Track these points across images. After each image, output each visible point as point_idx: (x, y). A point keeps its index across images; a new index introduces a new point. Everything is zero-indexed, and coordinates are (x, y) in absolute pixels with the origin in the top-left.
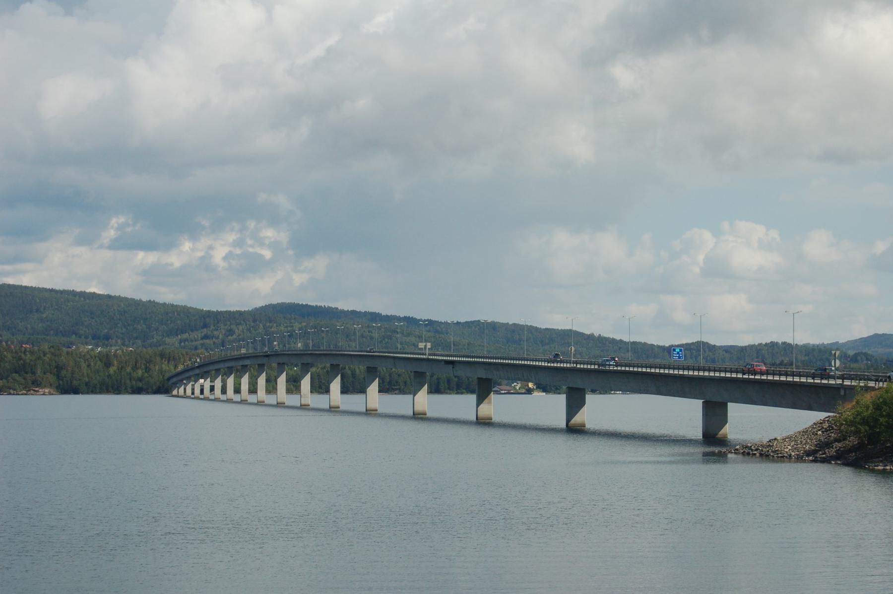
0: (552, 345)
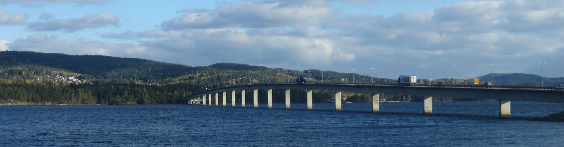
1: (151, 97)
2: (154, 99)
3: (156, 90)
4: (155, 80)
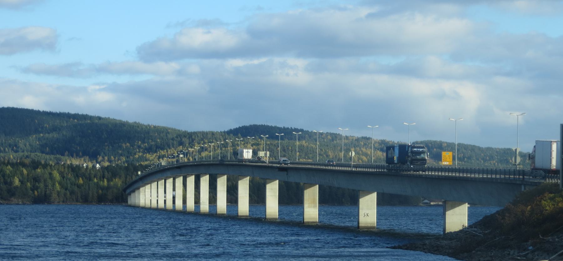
0: (492, 162)
1: (66, 189)
2: (71, 194)
3: (77, 176)
4: (112, 157)
